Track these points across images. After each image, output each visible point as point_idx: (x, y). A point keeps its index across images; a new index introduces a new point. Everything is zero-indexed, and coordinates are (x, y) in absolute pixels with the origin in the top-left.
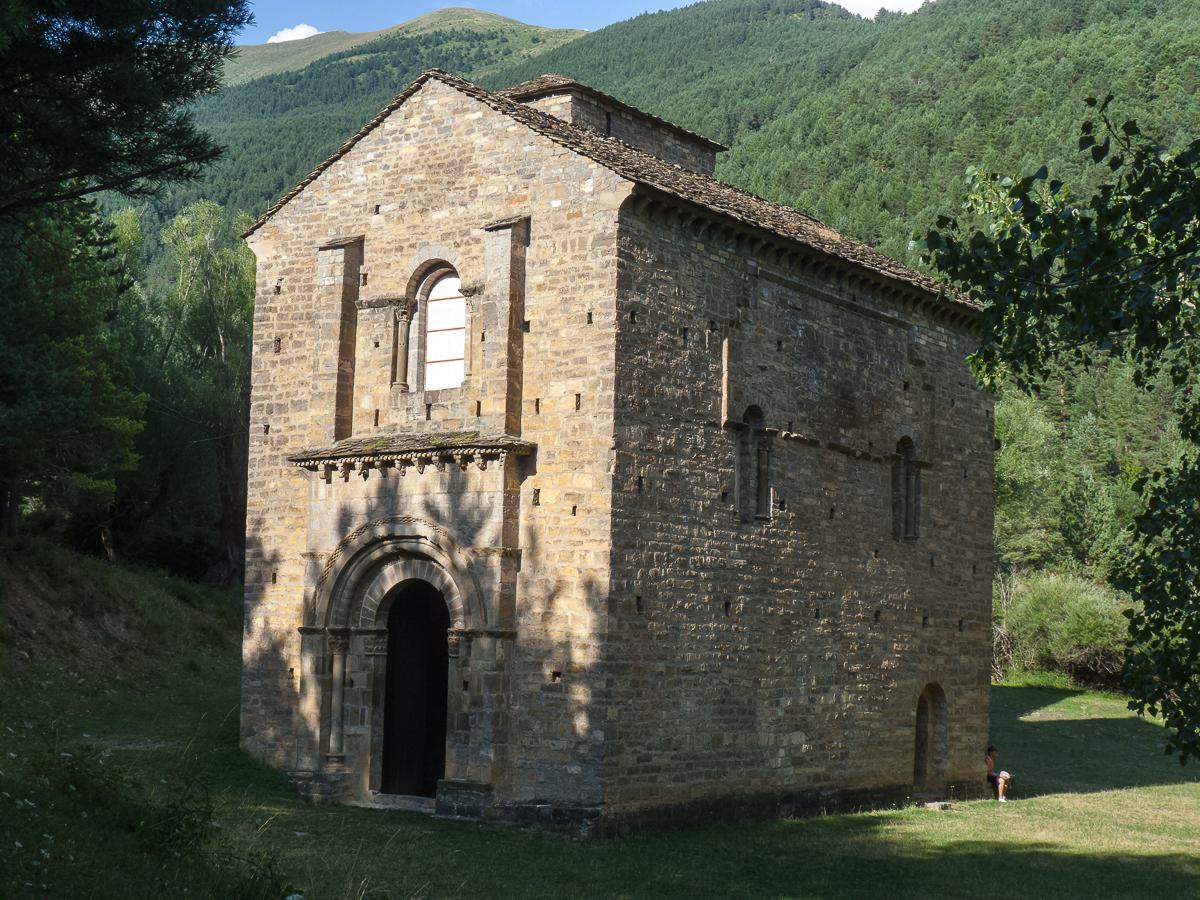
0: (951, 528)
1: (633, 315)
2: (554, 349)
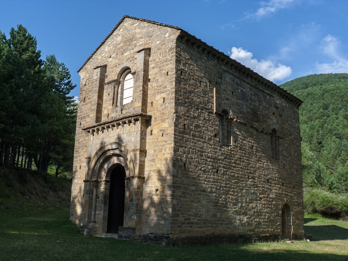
0: (289, 158)
1: (182, 72)
2: (157, 85)
